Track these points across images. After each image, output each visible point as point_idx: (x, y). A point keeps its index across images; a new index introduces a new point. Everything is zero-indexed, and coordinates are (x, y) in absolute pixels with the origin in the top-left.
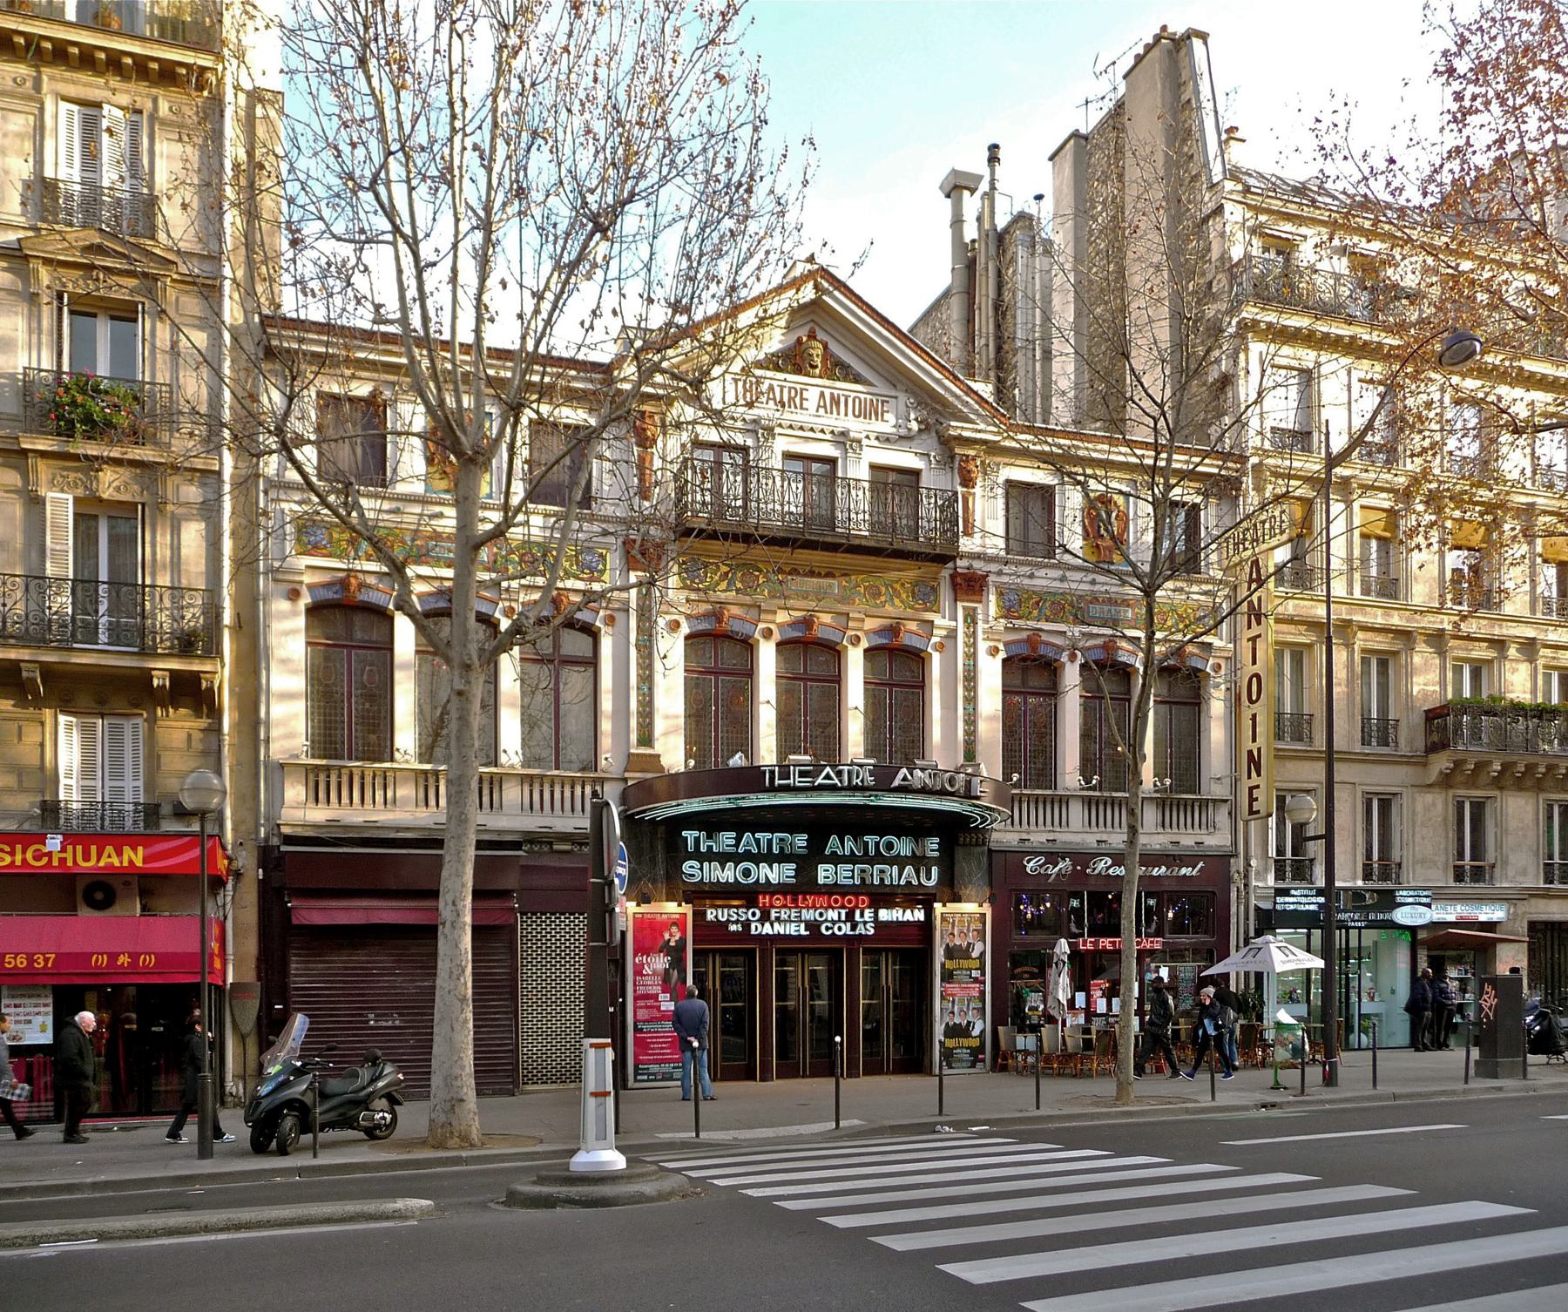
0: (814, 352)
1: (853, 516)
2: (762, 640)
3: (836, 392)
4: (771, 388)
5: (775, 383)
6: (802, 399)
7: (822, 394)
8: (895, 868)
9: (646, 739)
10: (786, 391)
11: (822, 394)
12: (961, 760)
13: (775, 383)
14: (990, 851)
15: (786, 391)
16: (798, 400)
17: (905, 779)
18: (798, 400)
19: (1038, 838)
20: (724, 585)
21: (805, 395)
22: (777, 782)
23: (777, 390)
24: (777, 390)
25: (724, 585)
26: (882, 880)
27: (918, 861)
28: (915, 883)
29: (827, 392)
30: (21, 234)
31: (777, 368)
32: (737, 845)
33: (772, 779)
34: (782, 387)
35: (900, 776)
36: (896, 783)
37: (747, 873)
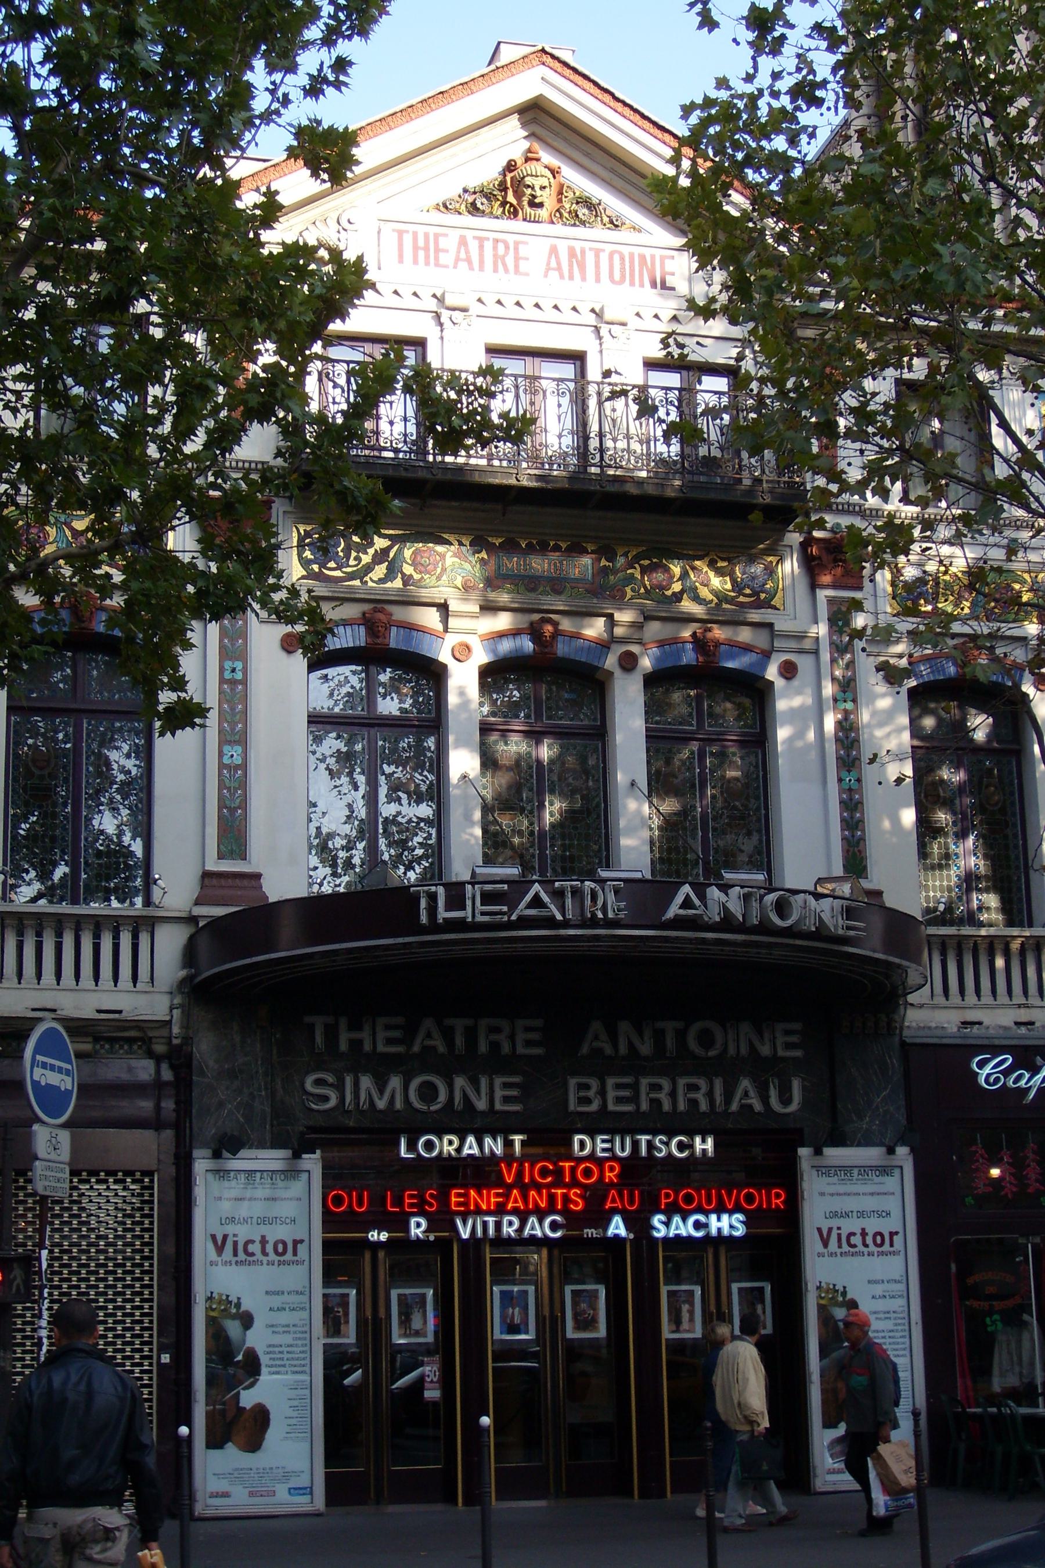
0: (537, 183)
1: (609, 444)
2: (618, 673)
3: (578, 246)
4: (463, 242)
5: (469, 235)
6: (517, 259)
7: (554, 250)
8: (718, 1084)
9: (233, 834)
10: (488, 246)
11: (554, 250)
12: (838, 870)
13: (469, 235)
14: (903, 1044)
15: (488, 246)
16: (510, 260)
17: (687, 904)
18: (510, 260)
19: (998, 1018)
20: (380, 571)
21: (523, 251)
22: (443, 914)
23: (473, 246)
24: (473, 246)
25: (380, 571)
26: (694, 1103)
27: (764, 1070)
28: (758, 1107)
29: (563, 247)
30: (631, 402)
31: (474, 209)
32: (407, 1040)
33: (432, 910)
34: (597, 253)
35: (679, 899)
36: (674, 910)
37: (428, 1092)
